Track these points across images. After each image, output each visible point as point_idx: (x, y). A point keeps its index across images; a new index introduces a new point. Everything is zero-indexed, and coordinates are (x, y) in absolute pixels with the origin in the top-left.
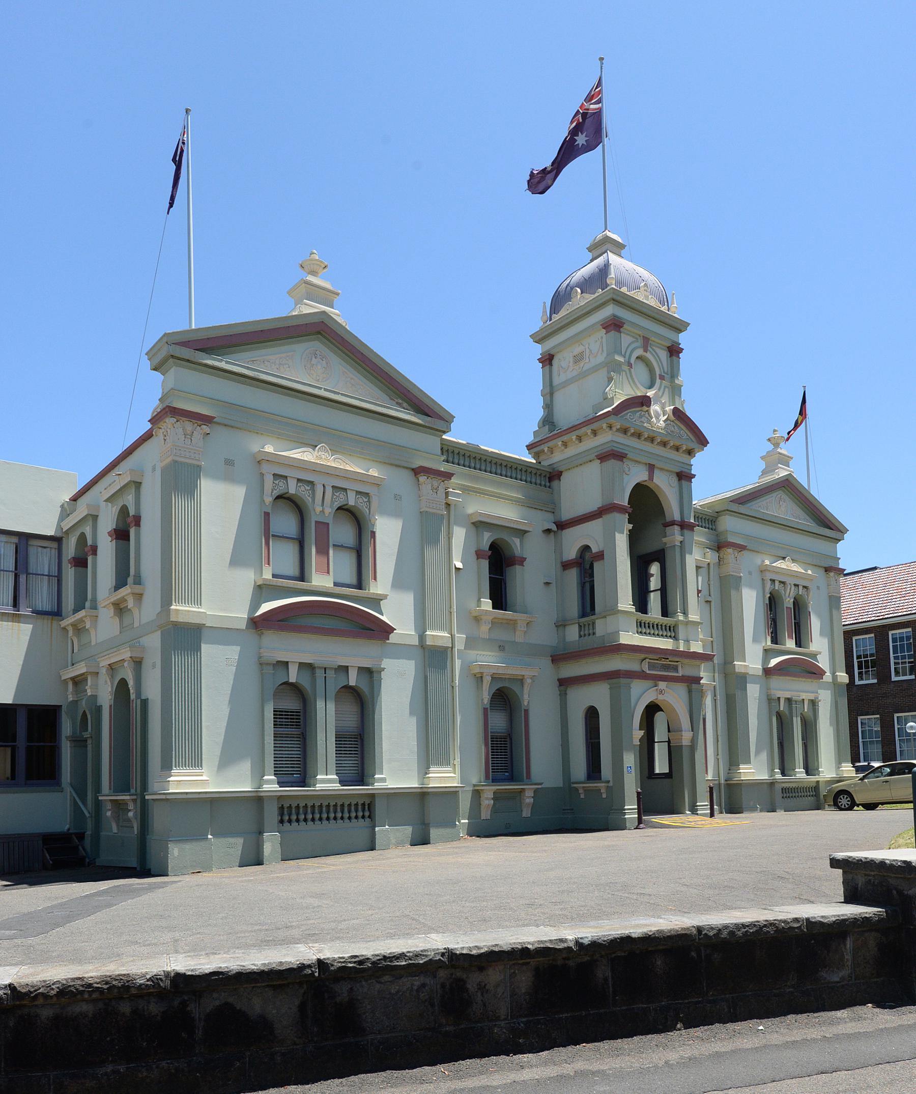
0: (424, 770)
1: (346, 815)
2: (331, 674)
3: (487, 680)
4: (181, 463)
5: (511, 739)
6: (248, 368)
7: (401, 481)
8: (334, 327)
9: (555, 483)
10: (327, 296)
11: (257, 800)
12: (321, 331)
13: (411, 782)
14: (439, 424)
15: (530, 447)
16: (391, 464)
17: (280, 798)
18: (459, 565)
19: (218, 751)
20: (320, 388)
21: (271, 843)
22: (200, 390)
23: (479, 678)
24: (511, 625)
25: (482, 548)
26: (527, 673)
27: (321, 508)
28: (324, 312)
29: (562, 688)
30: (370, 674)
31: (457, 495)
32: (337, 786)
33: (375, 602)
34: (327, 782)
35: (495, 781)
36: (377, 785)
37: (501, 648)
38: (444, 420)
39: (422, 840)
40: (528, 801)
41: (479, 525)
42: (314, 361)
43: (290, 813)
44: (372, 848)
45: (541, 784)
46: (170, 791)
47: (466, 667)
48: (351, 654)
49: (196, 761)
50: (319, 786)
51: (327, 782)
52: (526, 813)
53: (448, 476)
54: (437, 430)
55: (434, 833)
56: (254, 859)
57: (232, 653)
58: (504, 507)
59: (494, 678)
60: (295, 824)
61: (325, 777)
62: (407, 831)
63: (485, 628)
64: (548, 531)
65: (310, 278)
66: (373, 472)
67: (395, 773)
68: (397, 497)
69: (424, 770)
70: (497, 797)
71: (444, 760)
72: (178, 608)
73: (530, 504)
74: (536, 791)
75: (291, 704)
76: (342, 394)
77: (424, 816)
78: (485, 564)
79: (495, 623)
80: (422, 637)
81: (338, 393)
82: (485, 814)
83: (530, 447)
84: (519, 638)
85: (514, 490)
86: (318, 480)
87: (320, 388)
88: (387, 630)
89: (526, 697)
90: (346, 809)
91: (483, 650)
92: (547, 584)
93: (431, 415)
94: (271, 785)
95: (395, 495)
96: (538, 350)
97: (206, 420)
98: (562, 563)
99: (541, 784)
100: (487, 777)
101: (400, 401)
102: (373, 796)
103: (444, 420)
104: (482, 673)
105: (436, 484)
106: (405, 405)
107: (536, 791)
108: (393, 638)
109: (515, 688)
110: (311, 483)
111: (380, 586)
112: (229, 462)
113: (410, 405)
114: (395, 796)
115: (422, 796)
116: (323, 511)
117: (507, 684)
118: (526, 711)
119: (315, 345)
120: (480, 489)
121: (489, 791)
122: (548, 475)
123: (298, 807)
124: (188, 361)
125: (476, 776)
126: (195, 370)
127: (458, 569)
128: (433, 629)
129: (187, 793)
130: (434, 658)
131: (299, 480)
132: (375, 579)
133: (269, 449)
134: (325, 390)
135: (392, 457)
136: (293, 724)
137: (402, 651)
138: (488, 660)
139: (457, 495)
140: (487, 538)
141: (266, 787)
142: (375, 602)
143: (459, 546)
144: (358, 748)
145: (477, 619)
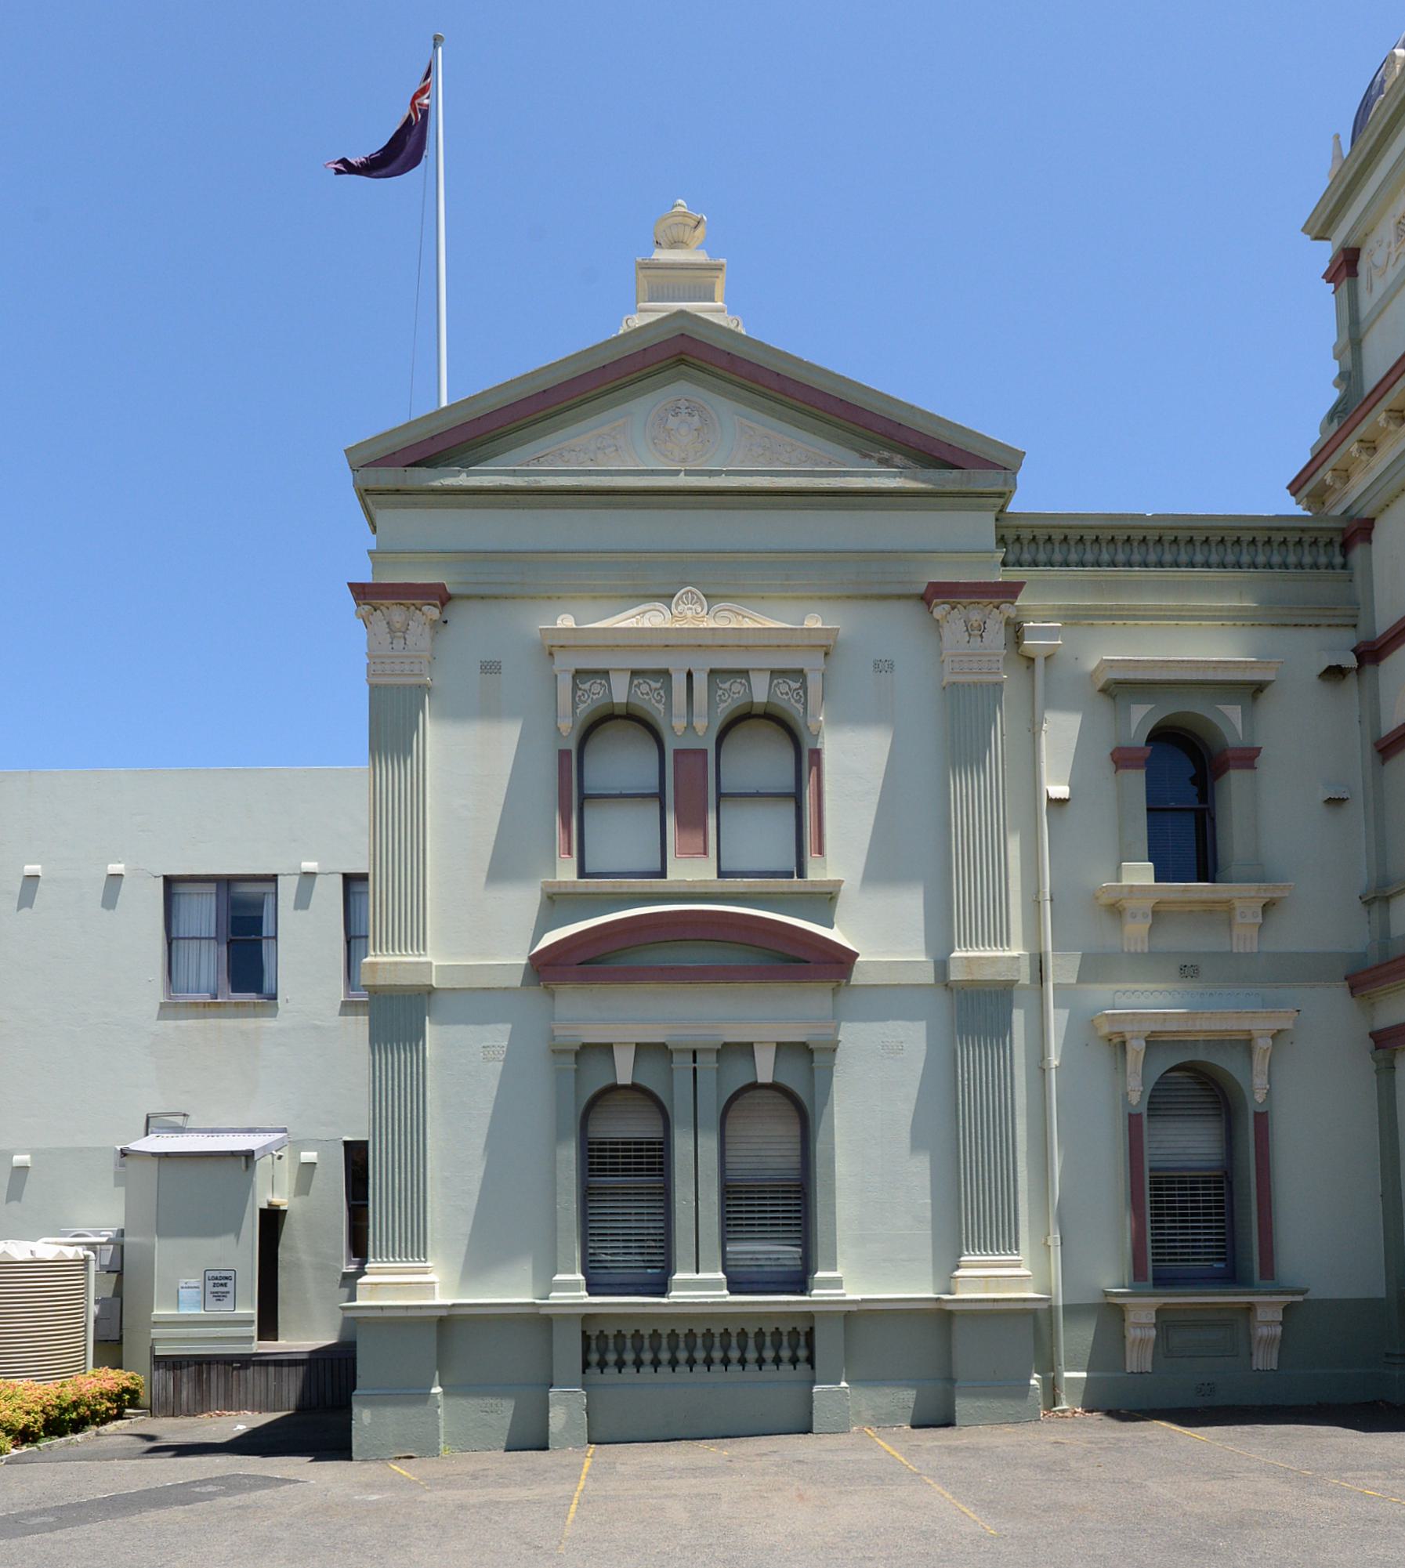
0: (948, 1261)
1: (751, 1355)
2: (707, 1063)
3: (1137, 1047)
4: (404, 686)
5: (1230, 1183)
6: (514, 473)
7: (890, 630)
8: (723, 344)
9: (1357, 553)
10: (697, 281)
11: (539, 1323)
12: (682, 355)
13: (915, 1288)
14: (982, 481)
15: (1295, 487)
16: (866, 597)
17: (587, 1318)
18: (1060, 791)
19: (465, 1225)
20: (676, 473)
21: (565, 1409)
22: (433, 538)
23: (1119, 1046)
24: (1221, 914)
25: (1126, 744)
26: (1261, 1025)
27: (690, 722)
28: (682, 313)
29: (1380, 1053)
30: (809, 1056)
31: (1052, 633)
32: (724, 1295)
33: (824, 902)
34: (698, 1287)
35: (1163, 1281)
36: (818, 1294)
37: (1188, 971)
38: (993, 466)
39: (937, 1416)
40: (1263, 1331)
41: (1119, 690)
42: (673, 422)
43: (603, 1348)
44: (807, 1430)
45: (1302, 1292)
46: (358, 1303)
47: (1083, 1027)
48: (763, 1018)
49: (415, 1246)
50: (676, 1295)
51: (698, 1287)
52: (1265, 1360)
53: (1011, 590)
54: (981, 495)
55: (962, 1406)
56: (531, 1437)
57: (498, 1036)
58: (1194, 637)
59: (1154, 1043)
60: (786, 1367)
61: (694, 1276)
62: (502, 1413)
63: (1136, 932)
64: (1334, 673)
65: (664, 255)
66: (813, 622)
67: (869, 1263)
68: (883, 666)
69: (948, 1261)
70: (1165, 1320)
71: (1001, 1235)
72: (379, 959)
73: (1279, 617)
74: (1288, 1309)
75: (1190, 1143)
76: (729, 473)
77: (945, 1364)
78: (1137, 779)
79: (1159, 915)
80: (942, 966)
81: (718, 473)
82: (1138, 1360)
83: (1295, 487)
84: (1244, 938)
85: (1232, 592)
86: (677, 666)
87: (676, 473)
88: (839, 961)
89: (1260, 1082)
90: (751, 1343)
91: (1136, 981)
92: (1334, 802)
93: (948, 461)
94: (570, 1291)
95: (877, 665)
96: (1324, 253)
97: (441, 597)
98: (1376, 744)
99: (1302, 1292)
100: (1138, 1274)
101: (886, 454)
102: (810, 1316)
103: (993, 466)
104: (1121, 1034)
105: (975, 616)
106: (898, 459)
107: (1288, 1309)
108: (858, 977)
109: (1228, 1063)
110: (665, 674)
111: (838, 863)
112: (490, 668)
113: (906, 455)
114: (857, 1318)
115: (942, 1320)
116: (690, 726)
117: (1201, 1056)
118: (1262, 1120)
119: (682, 390)
120: (1121, 608)
121: (1142, 1312)
122: (1338, 539)
123: (743, 1334)
124: (397, 491)
125: (1109, 1274)
126: (415, 505)
127: (1057, 803)
128: (970, 943)
129: (382, 1308)
130: (977, 1011)
131: (635, 673)
132: (820, 850)
133: (566, 621)
134: (688, 473)
135: (867, 582)
136: (618, 1166)
137: (891, 1000)
138: (1150, 1001)
139: (1052, 633)
140: (1141, 718)
141: (557, 1297)
142: (824, 902)
143: (1060, 752)
144: (781, 1207)
145: (1115, 911)
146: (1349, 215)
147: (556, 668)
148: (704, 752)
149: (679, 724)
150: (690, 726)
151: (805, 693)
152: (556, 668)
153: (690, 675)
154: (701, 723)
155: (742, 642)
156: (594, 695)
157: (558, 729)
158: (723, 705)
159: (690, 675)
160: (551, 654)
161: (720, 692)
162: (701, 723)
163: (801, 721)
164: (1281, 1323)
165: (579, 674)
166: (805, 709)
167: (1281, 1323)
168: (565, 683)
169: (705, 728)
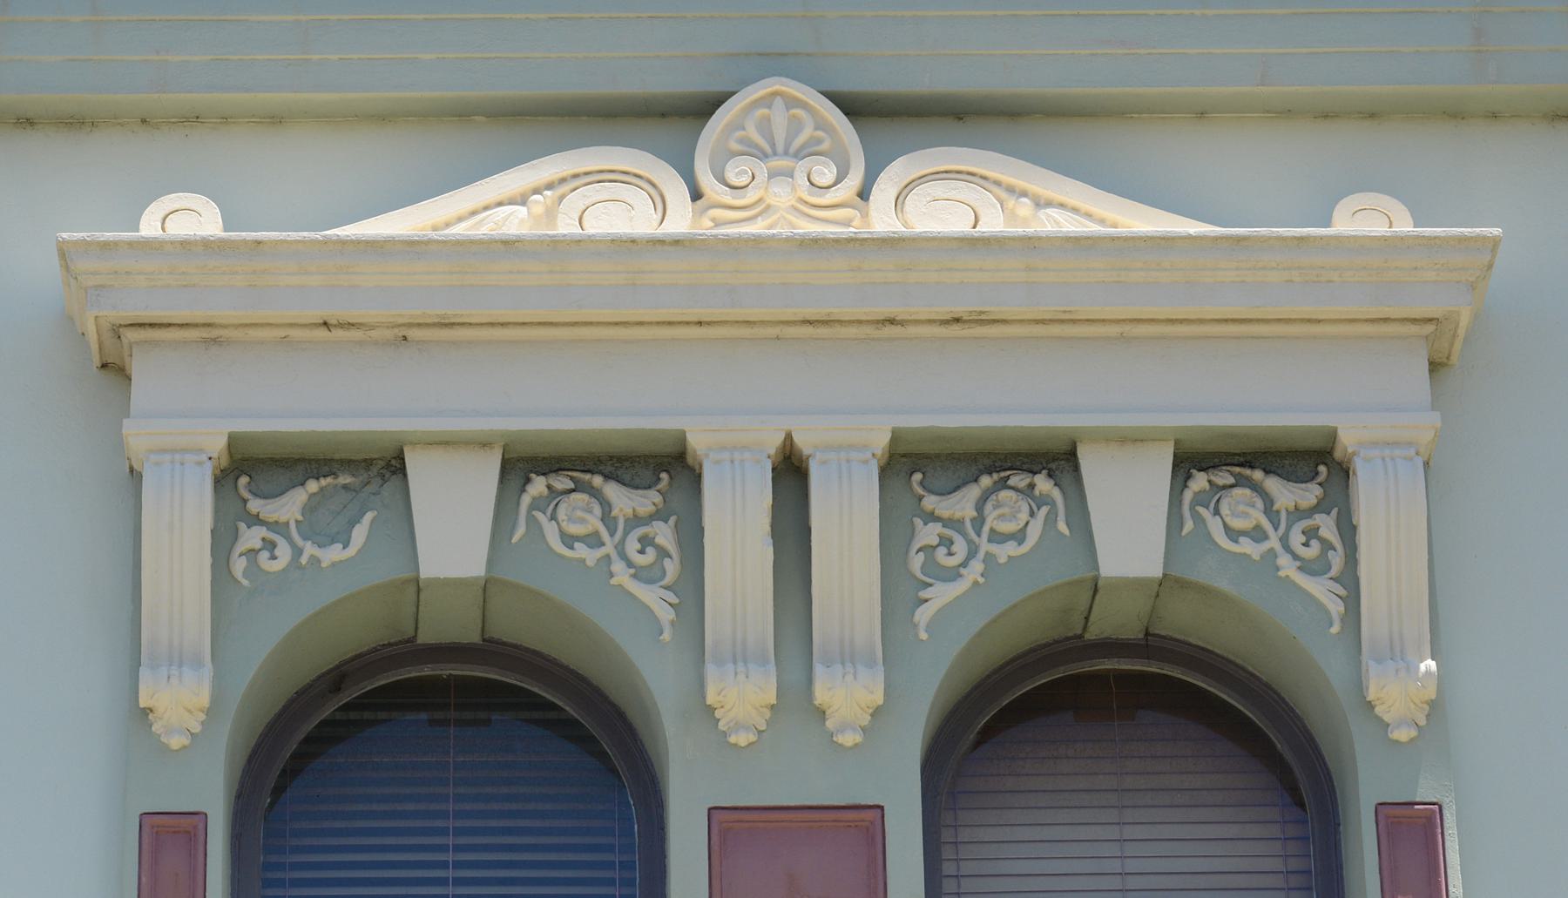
110: (667, 467)
116: (797, 703)
146: (539, 427)
147: (139, 435)
148: (864, 824)
149: (743, 696)
150: (797, 703)
151: (1348, 530)
152: (139, 435)
153: (791, 471)
154: (848, 696)
155: (962, 300)
156: (323, 576)
157: (145, 714)
158: (941, 595)
159: (791, 471)
160: (115, 369)
161: (928, 534)
162: (848, 696)
163: (1334, 669)
164: (863, 729)
165: (251, 468)
166: (1352, 600)
167: (863, 729)
168: (180, 515)
169: (864, 724)
